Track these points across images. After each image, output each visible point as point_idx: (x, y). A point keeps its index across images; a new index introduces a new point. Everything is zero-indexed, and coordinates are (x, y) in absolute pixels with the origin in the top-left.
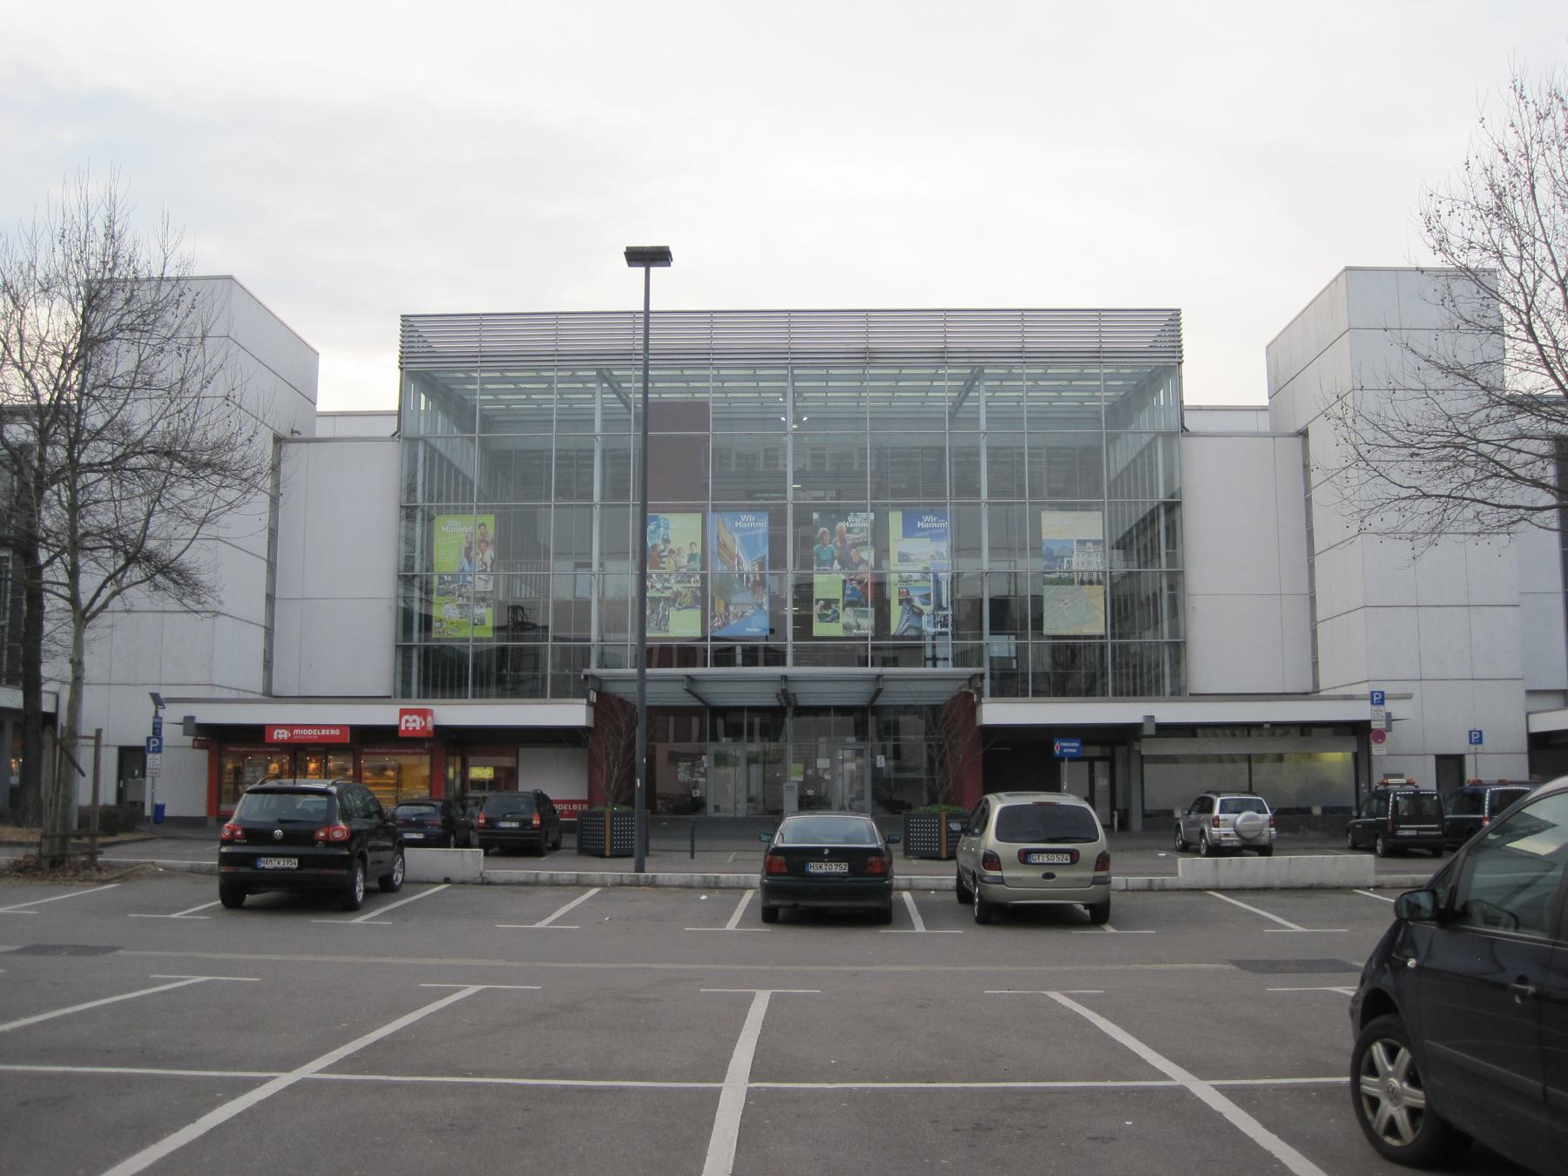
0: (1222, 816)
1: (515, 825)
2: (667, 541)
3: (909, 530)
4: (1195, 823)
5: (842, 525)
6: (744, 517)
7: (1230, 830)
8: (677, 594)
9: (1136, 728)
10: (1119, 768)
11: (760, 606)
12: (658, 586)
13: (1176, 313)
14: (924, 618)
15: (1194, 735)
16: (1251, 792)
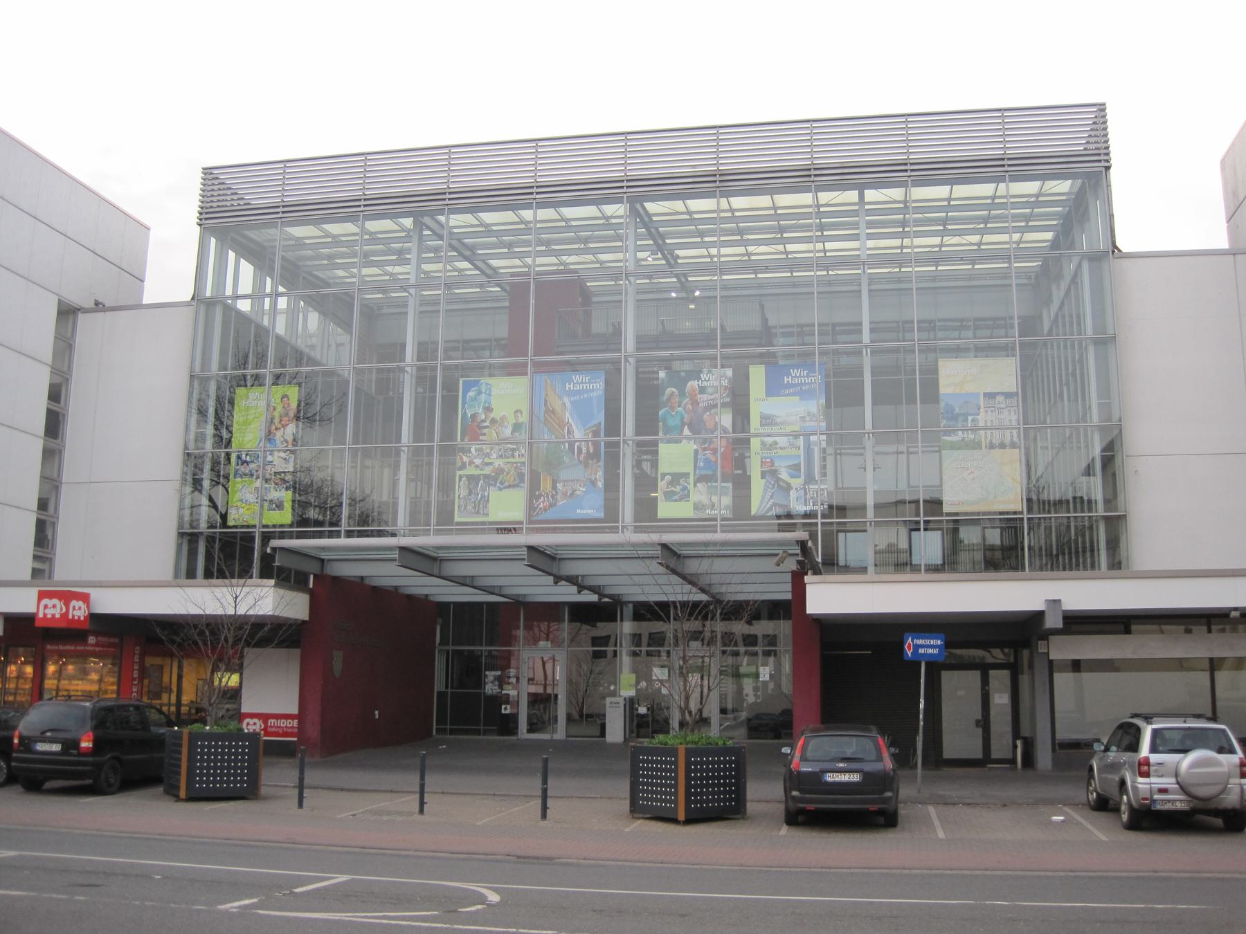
0: (1154, 758)
1: (56, 747)
2: (488, 409)
3: (773, 389)
4: (1114, 767)
5: (693, 384)
6: (577, 378)
7: (1168, 782)
8: (499, 471)
9: (1036, 618)
10: (1024, 680)
11: (594, 483)
12: (478, 461)
13: (1101, 108)
14: (793, 494)
15: (1128, 631)
16: (1214, 719)
